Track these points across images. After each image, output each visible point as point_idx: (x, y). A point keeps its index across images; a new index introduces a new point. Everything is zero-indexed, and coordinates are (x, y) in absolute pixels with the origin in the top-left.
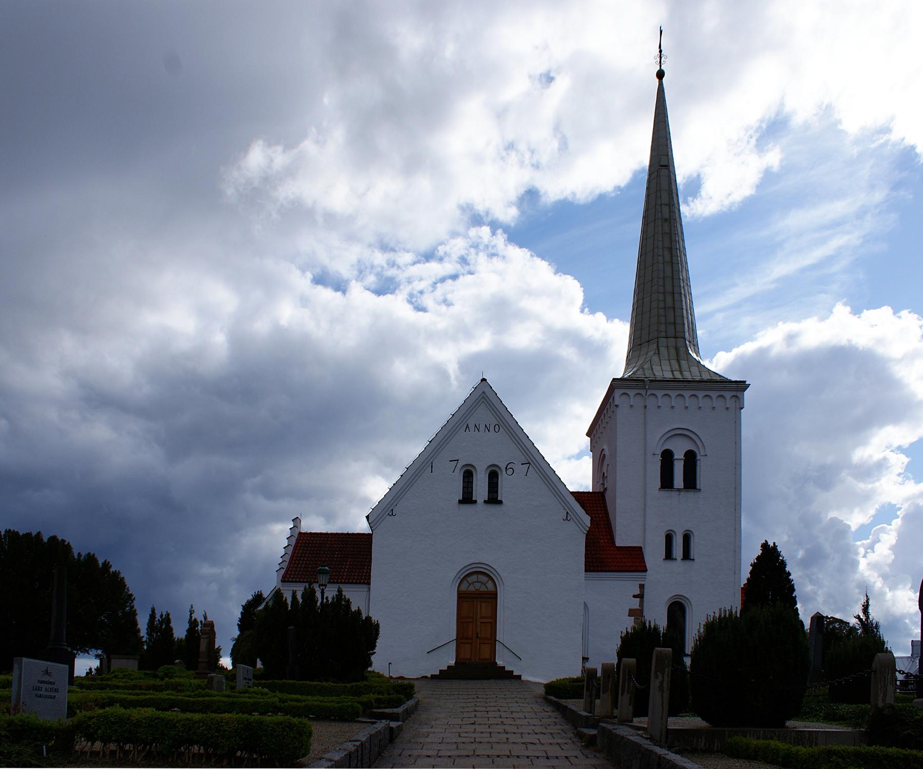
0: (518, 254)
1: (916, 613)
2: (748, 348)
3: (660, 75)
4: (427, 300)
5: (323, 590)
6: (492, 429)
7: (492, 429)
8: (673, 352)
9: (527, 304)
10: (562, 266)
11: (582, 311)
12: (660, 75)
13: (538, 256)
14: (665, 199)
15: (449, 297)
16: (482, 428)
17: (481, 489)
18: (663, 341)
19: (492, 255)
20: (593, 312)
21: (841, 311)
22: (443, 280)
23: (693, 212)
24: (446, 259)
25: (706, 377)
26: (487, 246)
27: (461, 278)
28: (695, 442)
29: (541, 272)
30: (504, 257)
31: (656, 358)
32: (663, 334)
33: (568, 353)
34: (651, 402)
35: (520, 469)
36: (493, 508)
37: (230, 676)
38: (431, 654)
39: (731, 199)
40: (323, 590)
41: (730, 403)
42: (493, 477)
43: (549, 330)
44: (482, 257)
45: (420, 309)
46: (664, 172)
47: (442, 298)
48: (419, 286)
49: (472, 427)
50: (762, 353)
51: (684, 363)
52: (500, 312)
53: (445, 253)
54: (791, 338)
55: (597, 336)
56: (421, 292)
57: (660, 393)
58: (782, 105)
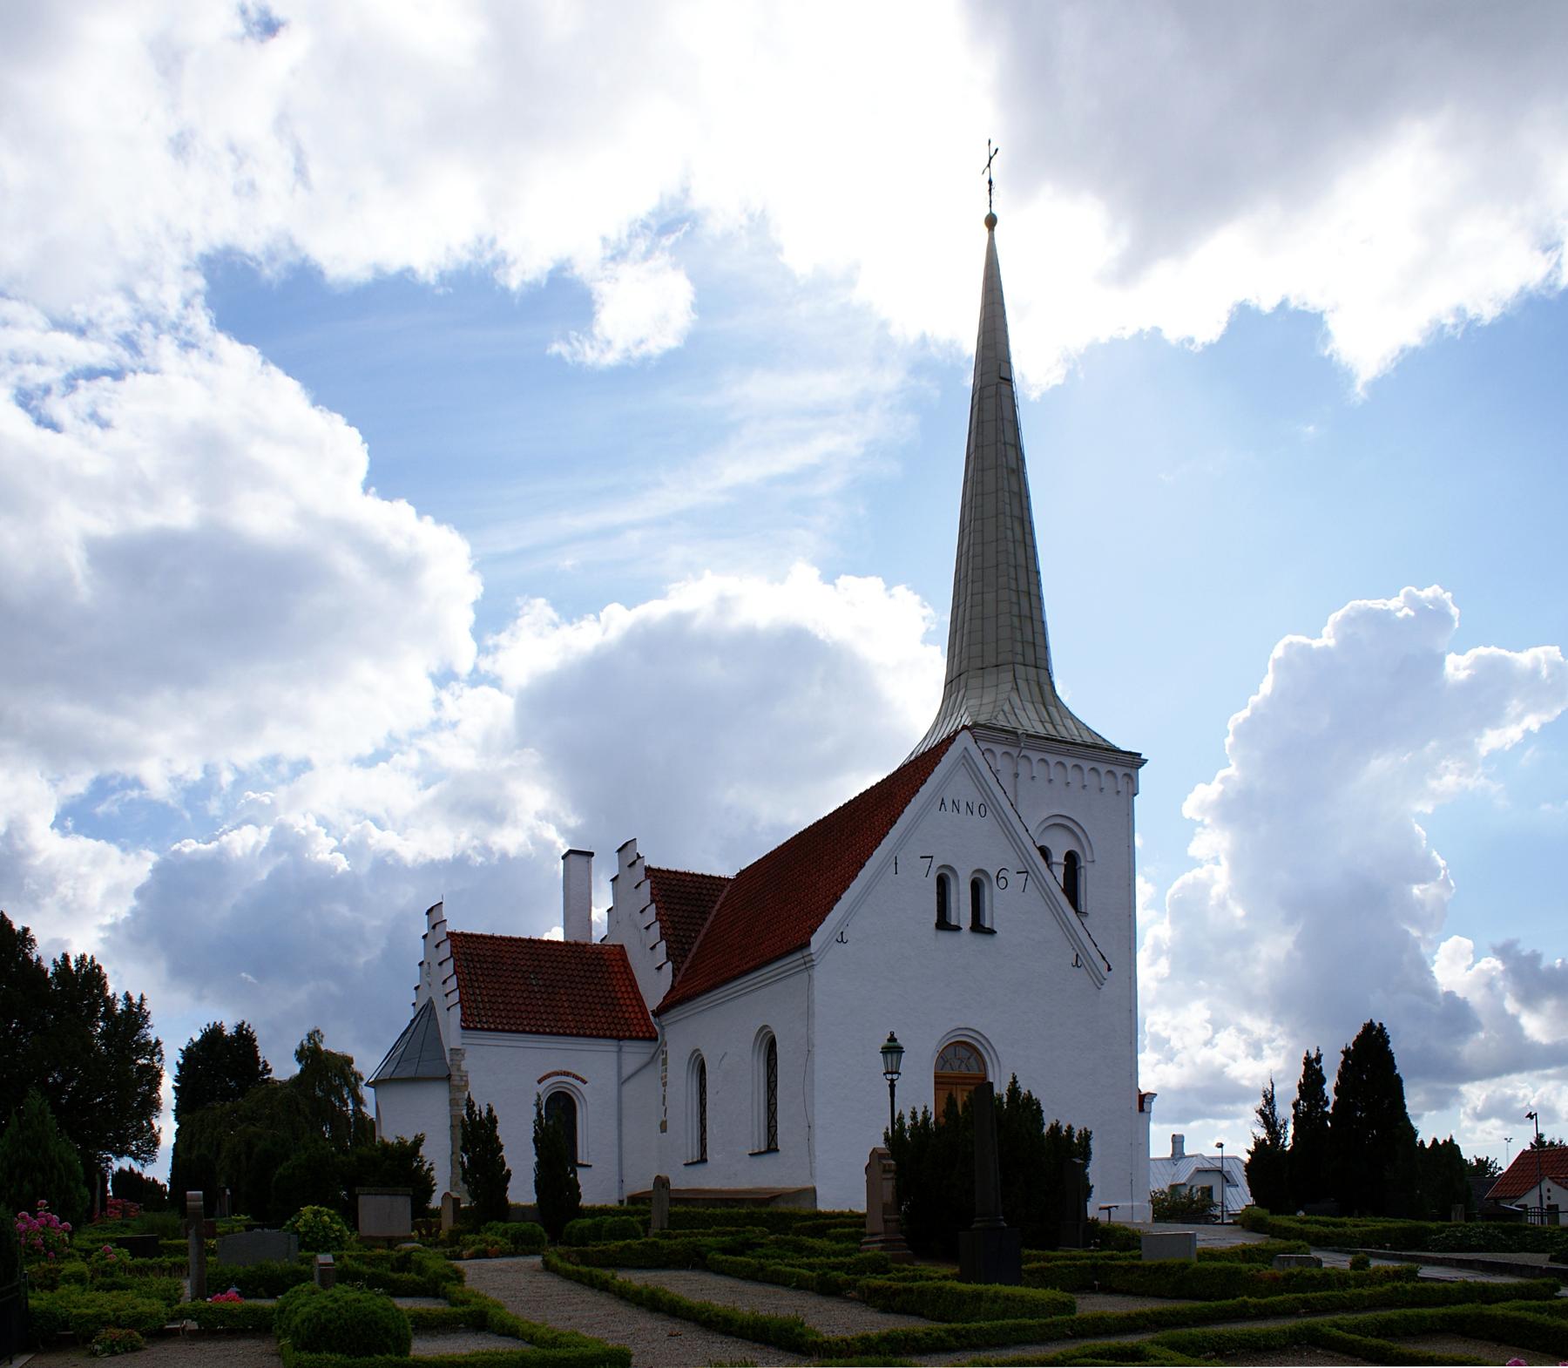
0: (239, 357)
1: (1418, 1117)
2: (656, 610)
3: (991, 222)
4: (59, 408)
5: (892, 1081)
6: (976, 810)
7: (976, 810)
8: (1035, 689)
9: (259, 451)
10: (324, 394)
11: (366, 490)
12: (991, 222)
13: (278, 364)
14: (1009, 437)
15: (104, 412)
16: (963, 807)
17: (961, 911)
18: (1020, 669)
19: (186, 346)
20: (387, 495)
21: (804, 574)
22: (92, 374)
23: (579, 358)
24: (91, 333)
25: (1089, 740)
26: (175, 327)
27: (130, 378)
28: (1078, 839)
29: (285, 398)
30: (211, 354)
31: (1014, 697)
32: (1020, 658)
33: (349, 564)
34: (1023, 768)
35: (1016, 881)
36: (981, 941)
37: (95, 1173)
38: (755, 1159)
39: (644, 349)
40: (892, 1081)
41: (1122, 784)
42: (976, 887)
43: (305, 515)
44: (167, 348)
45: (47, 423)
46: (1004, 387)
47: (88, 410)
48: (39, 376)
49: (948, 803)
50: (680, 621)
51: (1053, 710)
52: (209, 456)
53: (90, 321)
54: (724, 604)
55: (399, 545)
56: (47, 391)
57: (1035, 756)
58: (686, 191)
